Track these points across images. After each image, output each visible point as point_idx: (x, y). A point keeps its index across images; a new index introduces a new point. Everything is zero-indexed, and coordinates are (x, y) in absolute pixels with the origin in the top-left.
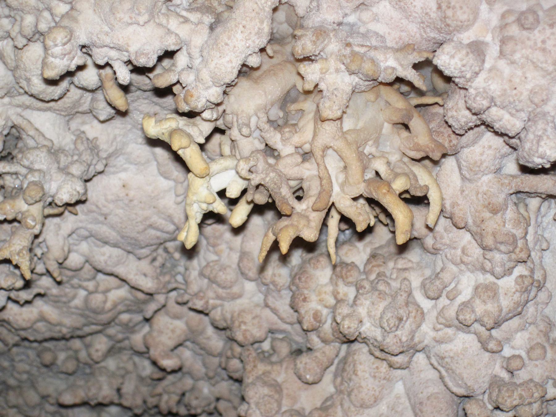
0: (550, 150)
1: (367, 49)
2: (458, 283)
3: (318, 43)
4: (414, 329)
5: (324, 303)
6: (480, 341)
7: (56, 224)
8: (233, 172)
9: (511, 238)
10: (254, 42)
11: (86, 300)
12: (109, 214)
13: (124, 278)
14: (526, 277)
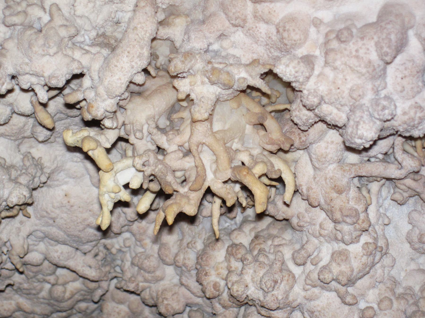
0: (366, 132)
1: (224, 65)
2: (320, 251)
3: (186, 62)
4: (288, 289)
5: (221, 276)
6: (339, 297)
7: (17, 227)
8: (133, 170)
9: (354, 212)
10: (136, 63)
11: (50, 292)
12: (57, 218)
13: (74, 270)
14: (370, 243)
